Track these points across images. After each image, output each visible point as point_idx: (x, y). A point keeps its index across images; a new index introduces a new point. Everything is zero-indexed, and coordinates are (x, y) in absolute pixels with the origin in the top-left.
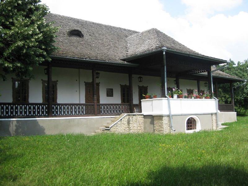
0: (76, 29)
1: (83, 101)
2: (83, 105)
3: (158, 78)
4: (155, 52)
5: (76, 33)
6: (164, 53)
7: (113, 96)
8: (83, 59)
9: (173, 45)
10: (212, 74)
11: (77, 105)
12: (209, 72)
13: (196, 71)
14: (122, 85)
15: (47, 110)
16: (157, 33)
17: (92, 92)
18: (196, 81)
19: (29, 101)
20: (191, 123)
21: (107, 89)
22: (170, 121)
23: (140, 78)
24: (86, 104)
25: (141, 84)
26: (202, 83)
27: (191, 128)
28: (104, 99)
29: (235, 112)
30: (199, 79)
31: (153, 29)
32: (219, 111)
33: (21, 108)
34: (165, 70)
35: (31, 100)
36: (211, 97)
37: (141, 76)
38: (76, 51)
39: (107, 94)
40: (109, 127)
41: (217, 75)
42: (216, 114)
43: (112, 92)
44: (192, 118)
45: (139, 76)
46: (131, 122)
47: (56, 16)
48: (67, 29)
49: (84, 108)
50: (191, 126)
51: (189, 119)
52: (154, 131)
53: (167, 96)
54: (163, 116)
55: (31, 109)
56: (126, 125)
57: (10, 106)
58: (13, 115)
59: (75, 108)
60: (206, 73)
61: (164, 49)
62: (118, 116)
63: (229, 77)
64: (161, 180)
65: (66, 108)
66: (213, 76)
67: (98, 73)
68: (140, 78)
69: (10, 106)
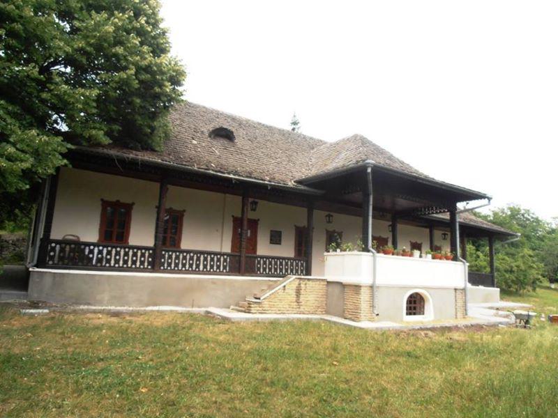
0: (230, 128)
1: (227, 248)
2: (228, 255)
3: (360, 220)
4: (353, 168)
5: (223, 133)
6: (369, 170)
7: (280, 244)
8: (224, 173)
9: (388, 161)
10: (459, 219)
11: (216, 254)
12: (453, 212)
13: (428, 210)
14: (183, 215)
15: (150, 259)
16: (364, 142)
17: (244, 234)
18: (428, 230)
19: (129, 241)
20: (415, 304)
21: (271, 231)
22: (372, 296)
23: (329, 216)
24: (233, 254)
25: (331, 227)
26: (438, 233)
27: (414, 311)
28: (264, 248)
29: (497, 287)
30: (433, 225)
31: (355, 137)
32: (469, 285)
33: (118, 253)
34: (371, 202)
35: (133, 240)
36: (455, 259)
37: (331, 214)
38: (206, 157)
39: (271, 240)
40: (259, 299)
41: (467, 221)
42: (464, 290)
43: (280, 236)
44: (417, 294)
45: (327, 213)
46: (302, 292)
47: (195, 107)
48: (211, 127)
49: (228, 260)
50: (415, 308)
51: (411, 296)
52: (344, 311)
53: (371, 249)
54: (360, 286)
55: (144, 257)
56: (293, 297)
57: (216, 257)
58: (144, 268)
59: (205, 259)
60: (446, 216)
61: (369, 163)
62: (281, 279)
63: (488, 227)
64: (399, 363)
65: (262, 262)
66: (459, 222)
67: (256, 203)
68: (329, 216)
69: (147, 252)
